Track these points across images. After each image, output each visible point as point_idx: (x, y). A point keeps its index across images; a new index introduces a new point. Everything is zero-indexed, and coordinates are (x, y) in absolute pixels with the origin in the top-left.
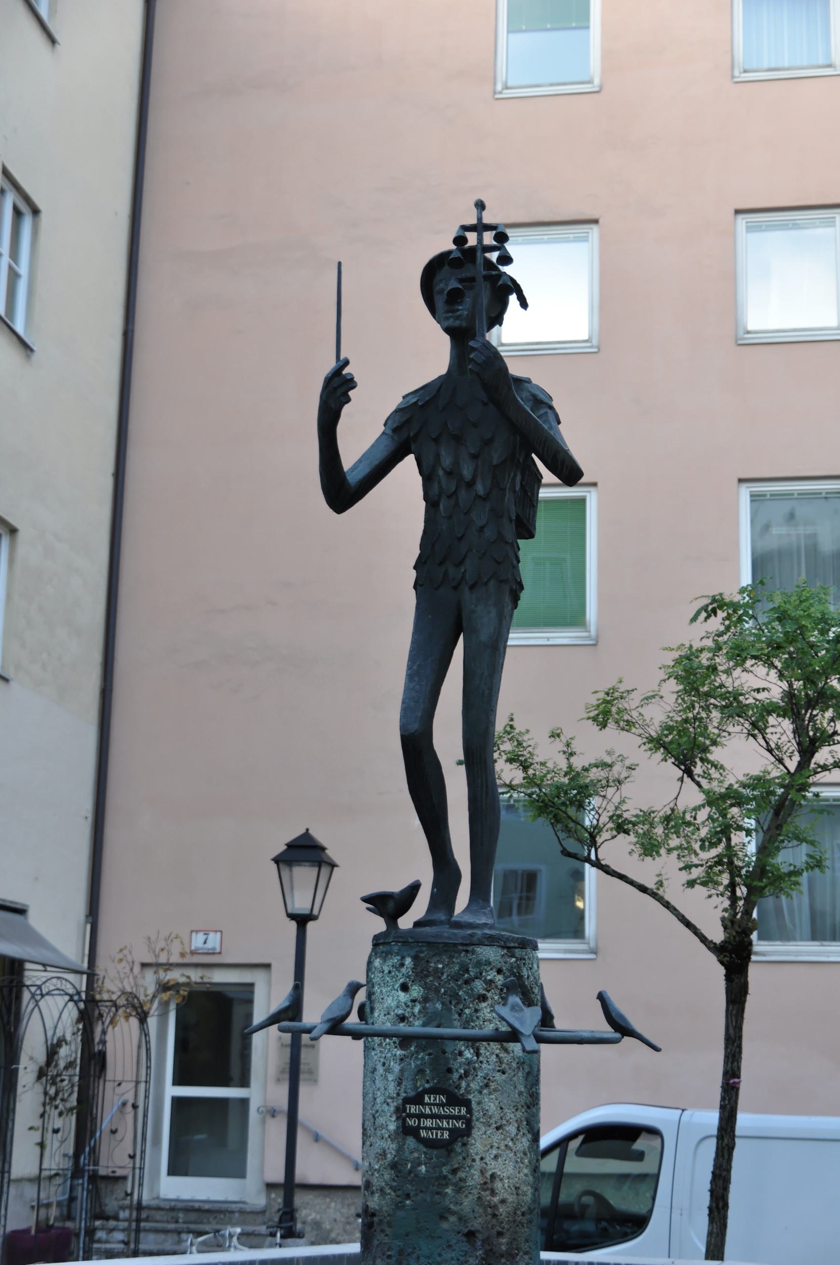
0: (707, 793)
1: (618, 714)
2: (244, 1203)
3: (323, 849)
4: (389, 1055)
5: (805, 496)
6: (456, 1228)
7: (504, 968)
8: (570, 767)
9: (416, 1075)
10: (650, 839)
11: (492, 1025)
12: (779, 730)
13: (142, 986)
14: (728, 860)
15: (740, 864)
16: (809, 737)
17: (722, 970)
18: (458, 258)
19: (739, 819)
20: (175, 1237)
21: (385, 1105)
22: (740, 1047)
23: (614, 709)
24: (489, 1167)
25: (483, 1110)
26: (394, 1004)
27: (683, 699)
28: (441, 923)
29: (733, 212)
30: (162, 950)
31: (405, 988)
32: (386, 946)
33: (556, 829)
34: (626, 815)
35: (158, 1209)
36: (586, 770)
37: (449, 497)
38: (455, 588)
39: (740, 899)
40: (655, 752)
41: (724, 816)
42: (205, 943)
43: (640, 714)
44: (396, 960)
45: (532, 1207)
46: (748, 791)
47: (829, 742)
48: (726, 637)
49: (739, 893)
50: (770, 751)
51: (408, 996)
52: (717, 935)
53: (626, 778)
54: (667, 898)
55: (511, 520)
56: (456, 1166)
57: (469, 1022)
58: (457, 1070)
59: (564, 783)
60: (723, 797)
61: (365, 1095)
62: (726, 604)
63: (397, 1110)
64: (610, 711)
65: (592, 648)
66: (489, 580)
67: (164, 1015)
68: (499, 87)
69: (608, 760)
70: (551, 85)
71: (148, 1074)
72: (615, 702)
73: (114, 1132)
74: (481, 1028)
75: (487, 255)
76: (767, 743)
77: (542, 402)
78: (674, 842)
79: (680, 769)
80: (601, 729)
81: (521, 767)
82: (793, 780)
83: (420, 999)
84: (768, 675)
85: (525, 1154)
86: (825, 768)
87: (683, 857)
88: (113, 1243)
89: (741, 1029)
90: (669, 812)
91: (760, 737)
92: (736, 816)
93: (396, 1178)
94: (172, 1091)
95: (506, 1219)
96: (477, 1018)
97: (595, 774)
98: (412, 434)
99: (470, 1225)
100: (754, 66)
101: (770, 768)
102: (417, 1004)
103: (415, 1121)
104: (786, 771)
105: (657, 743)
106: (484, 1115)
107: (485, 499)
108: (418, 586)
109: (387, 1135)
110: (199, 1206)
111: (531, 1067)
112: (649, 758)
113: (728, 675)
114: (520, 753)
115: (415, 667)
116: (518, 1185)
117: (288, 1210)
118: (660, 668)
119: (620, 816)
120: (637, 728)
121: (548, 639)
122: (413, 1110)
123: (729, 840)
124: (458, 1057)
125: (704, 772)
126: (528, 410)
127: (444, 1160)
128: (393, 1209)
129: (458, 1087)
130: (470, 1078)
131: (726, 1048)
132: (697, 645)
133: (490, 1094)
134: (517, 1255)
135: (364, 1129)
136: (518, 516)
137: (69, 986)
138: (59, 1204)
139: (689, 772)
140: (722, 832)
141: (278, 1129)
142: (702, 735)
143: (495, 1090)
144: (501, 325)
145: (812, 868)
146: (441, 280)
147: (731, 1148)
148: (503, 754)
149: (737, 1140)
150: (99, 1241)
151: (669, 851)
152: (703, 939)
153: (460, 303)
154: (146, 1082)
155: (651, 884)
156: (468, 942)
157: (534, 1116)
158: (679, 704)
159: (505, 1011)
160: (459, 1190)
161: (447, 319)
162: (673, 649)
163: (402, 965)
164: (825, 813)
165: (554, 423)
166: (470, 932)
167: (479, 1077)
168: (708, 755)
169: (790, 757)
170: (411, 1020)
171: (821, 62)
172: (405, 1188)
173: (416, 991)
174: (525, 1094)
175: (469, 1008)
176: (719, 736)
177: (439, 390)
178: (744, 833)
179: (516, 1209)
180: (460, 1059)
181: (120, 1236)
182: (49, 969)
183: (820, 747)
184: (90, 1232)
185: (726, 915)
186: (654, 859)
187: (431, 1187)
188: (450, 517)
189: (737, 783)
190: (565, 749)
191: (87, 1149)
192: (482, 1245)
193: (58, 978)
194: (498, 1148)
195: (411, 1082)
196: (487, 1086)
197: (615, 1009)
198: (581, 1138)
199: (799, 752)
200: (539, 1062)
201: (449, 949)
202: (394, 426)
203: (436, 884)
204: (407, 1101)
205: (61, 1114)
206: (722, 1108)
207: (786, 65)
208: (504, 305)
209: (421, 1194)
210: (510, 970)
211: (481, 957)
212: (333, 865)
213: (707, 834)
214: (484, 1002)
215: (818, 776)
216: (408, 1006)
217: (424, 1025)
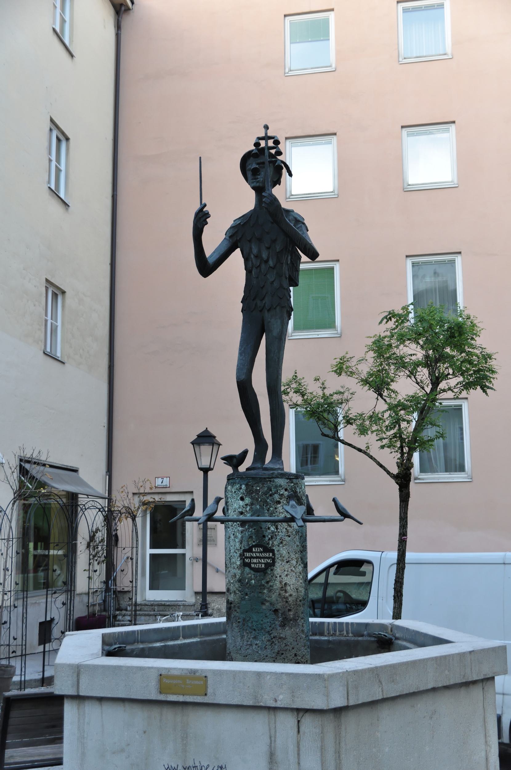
0: (389, 404)
1: (346, 368)
2: (185, 601)
3: (215, 437)
4: (236, 530)
5: (437, 262)
6: (269, 608)
7: (288, 488)
8: (324, 394)
9: (249, 539)
10: (363, 427)
11: (283, 515)
12: (422, 373)
13: (133, 503)
14: (399, 436)
15: (405, 437)
16: (436, 376)
17: (397, 487)
18: (256, 153)
19: (404, 416)
20: (154, 618)
21: (235, 553)
22: (406, 522)
23: (344, 367)
24: (283, 580)
25: (280, 554)
26: (237, 507)
27: (376, 361)
28: (259, 468)
29: (401, 127)
30: (141, 486)
31: (242, 499)
32: (233, 480)
33: (319, 424)
34: (350, 416)
35: (146, 605)
36: (331, 395)
37: (257, 268)
38: (261, 311)
39: (405, 453)
40: (365, 386)
41: (397, 415)
42: (162, 483)
43: (356, 368)
44: (237, 486)
45: (305, 598)
46: (408, 403)
47: (445, 379)
48: (396, 331)
49: (405, 451)
50: (418, 383)
51: (244, 503)
52: (395, 470)
53: (350, 399)
54: (371, 454)
55: (286, 278)
56: (269, 580)
57: (272, 514)
58: (267, 536)
59: (321, 402)
60: (397, 406)
61: (226, 549)
62: (395, 315)
63: (240, 555)
64: (342, 368)
65: (339, 338)
66: (276, 307)
67: (144, 516)
68: (287, 71)
69: (342, 390)
70: (312, 68)
71: (137, 544)
72: (345, 363)
73: (122, 571)
74: (278, 516)
75: (271, 151)
76: (416, 380)
77: (299, 221)
78: (375, 428)
79: (377, 393)
80: (339, 376)
81: (301, 395)
82: (429, 397)
83: (249, 504)
84: (417, 348)
85: (300, 573)
86: (444, 391)
87: (379, 434)
88: (125, 621)
89: (407, 513)
90: (372, 414)
91: (413, 377)
92: (402, 415)
93: (241, 586)
94: (150, 551)
95: (292, 603)
96: (276, 512)
97: (336, 397)
98: (238, 239)
99: (276, 606)
100: (409, 56)
101: (418, 392)
102: (248, 506)
103: (249, 560)
104: (425, 393)
105: (365, 382)
106: (281, 556)
107: (273, 268)
108: (244, 312)
109: (236, 567)
110: (164, 603)
111: (302, 533)
112: (362, 389)
113: (397, 348)
114: (300, 388)
115: (243, 349)
116: (298, 588)
117: (204, 604)
118: (366, 346)
119: (348, 416)
120: (355, 375)
121: (318, 335)
122: (247, 555)
123: (400, 426)
124: (268, 530)
125: (388, 395)
126: (292, 225)
127: (262, 578)
128: (240, 601)
129: (268, 544)
130: (274, 539)
131: (400, 523)
132: (383, 335)
133: (283, 546)
134: (298, 619)
135: (226, 565)
136: (290, 276)
137: (98, 504)
138: (99, 604)
139: (381, 395)
140: (396, 422)
141: (199, 567)
142: (387, 377)
143: (285, 545)
144: (279, 185)
145: (439, 438)
146: (250, 164)
147: (403, 569)
148: (292, 389)
149: (406, 565)
150: (119, 621)
151: (372, 432)
152: (388, 473)
153: (259, 175)
154: (136, 547)
155: (363, 448)
156: (271, 477)
157: (304, 556)
158: (375, 363)
159: (288, 508)
160: (270, 591)
161: (253, 182)
162: (372, 337)
163: (241, 488)
164: (445, 412)
165: (305, 231)
166: (272, 472)
167: (278, 539)
168: (390, 386)
169: (427, 386)
170: (245, 513)
171: (441, 53)
172: (245, 591)
173: (247, 500)
174: (300, 546)
175: (272, 507)
176: (394, 377)
177: (250, 217)
178: (406, 422)
179: (297, 599)
180: (269, 531)
181: (128, 618)
182: (89, 497)
183: (441, 381)
184: (115, 617)
185: (399, 461)
186: (365, 436)
187: (257, 590)
188: (257, 278)
189: (403, 399)
190: (322, 386)
191: (112, 578)
192: (281, 615)
193: (93, 501)
194: (288, 571)
195: (246, 542)
196: (282, 543)
197: (341, 506)
198: (336, 566)
199: (431, 384)
200: (306, 531)
201: (262, 480)
202: (230, 235)
203: (256, 450)
204: (245, 551)
205: (98, 564)
206: (399, 550)
207: (425, 55)
208: (280, 175)
209: (253, 593)
210: (291, 489)
211: (277, 483)
212: (219, 445)
213: (389, 423)
214: (279, 504)
215: (441, 394)
216: (244, 507)
217: (251, 516)
